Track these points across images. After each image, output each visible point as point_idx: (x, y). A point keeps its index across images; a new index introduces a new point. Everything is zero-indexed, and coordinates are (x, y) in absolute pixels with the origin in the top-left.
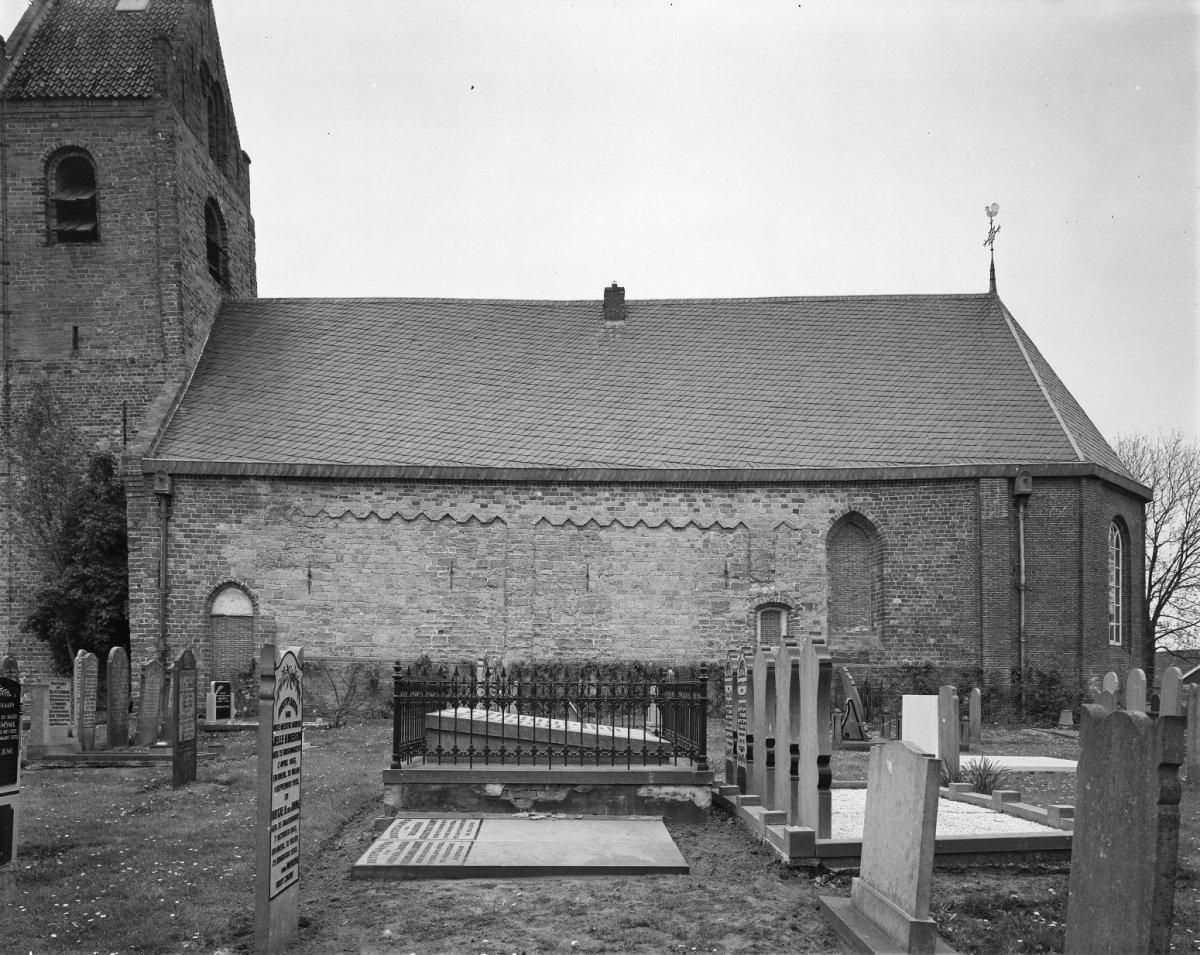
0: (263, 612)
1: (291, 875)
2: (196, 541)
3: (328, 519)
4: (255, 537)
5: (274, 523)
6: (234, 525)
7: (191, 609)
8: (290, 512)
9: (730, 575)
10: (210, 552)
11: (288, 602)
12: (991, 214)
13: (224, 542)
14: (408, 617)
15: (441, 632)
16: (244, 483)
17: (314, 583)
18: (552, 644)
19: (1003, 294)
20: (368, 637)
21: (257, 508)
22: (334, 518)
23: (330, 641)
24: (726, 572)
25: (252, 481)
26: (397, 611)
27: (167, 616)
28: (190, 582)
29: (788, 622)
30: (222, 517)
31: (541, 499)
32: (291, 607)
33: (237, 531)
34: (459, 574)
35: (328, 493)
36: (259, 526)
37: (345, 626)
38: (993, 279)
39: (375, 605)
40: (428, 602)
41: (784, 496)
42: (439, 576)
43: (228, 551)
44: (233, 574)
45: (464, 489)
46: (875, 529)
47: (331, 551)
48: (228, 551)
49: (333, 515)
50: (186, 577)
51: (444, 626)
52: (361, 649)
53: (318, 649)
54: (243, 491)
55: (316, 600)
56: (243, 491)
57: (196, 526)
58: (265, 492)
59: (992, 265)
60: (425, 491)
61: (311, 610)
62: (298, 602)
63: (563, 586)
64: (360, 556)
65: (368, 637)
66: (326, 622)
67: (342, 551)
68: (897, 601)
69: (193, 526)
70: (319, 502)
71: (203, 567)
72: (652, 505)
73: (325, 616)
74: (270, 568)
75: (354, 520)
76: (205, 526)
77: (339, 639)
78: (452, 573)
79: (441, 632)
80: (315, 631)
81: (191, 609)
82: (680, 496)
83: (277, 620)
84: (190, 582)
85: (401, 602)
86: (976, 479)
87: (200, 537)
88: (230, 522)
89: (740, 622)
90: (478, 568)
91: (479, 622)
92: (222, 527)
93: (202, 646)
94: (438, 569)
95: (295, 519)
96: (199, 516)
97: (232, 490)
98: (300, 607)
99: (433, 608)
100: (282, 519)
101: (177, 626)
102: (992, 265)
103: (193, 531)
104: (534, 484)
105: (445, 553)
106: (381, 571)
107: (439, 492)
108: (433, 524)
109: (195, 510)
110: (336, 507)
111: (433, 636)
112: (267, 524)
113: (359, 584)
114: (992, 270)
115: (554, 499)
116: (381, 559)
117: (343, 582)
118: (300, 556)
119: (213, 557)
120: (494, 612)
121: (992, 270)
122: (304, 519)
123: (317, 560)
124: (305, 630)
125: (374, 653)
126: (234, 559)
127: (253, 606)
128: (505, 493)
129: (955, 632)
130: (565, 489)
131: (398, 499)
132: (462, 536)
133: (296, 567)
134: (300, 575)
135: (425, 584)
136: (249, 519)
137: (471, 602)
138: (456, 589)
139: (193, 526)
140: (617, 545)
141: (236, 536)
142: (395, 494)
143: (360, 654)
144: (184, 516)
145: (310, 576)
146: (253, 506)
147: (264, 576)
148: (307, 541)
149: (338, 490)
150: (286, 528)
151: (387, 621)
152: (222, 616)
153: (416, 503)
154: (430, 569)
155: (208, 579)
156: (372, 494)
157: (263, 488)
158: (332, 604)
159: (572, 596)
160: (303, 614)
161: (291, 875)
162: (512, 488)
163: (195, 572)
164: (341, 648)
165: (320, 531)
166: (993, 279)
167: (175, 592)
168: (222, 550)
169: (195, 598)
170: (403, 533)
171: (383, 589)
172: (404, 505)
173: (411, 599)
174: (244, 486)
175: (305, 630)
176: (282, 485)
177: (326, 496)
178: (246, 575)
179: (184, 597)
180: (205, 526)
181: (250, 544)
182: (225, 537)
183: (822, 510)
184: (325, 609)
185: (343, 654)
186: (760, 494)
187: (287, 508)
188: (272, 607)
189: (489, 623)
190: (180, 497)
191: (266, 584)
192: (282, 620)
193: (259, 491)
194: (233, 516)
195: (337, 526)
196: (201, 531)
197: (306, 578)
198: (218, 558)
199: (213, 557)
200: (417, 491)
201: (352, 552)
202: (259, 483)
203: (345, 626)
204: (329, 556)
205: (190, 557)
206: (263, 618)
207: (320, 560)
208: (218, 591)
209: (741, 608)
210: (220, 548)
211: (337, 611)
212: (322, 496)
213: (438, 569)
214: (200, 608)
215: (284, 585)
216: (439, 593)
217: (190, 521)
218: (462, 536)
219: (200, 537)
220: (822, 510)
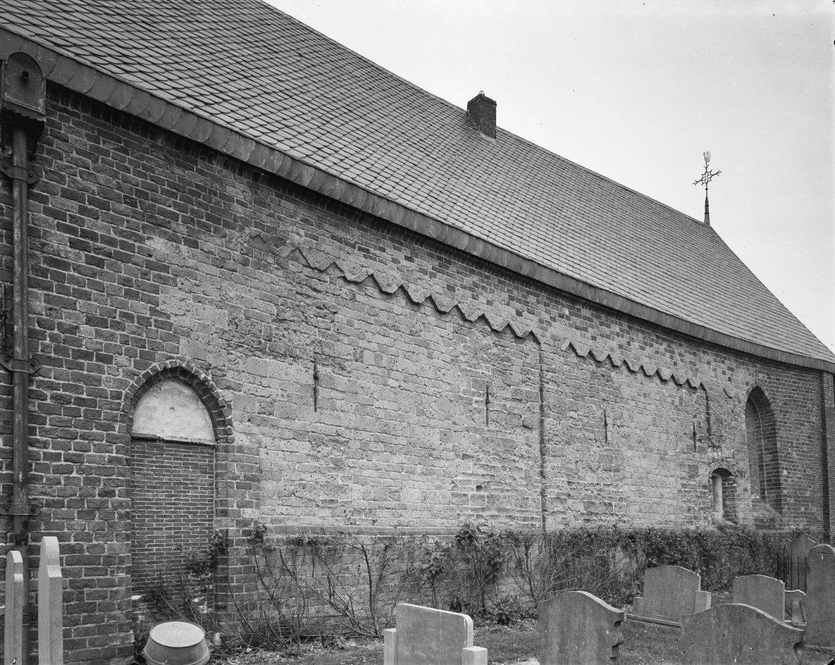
0: (239, 439)
1: (149, 546)
2: (100, 263)
3: (341, 281)
4: (225, 284)
5: (258, 266)
6: (183, 247)
7: (92, 418)
8: (285, 252)
9: (698, 437)
10: (133, 295)
11: (283, 422)
12: (707, 160)
13: (165, 281)
14: (442, 463)
15: (479, 488)
16: (201, 165)
17: (323, 393)
18: (581, 508)
19: (712, 224)
20: (394, 494)
21: (227, 225)
22: (350, 282)
23: (341, 498)
24: (695, 434)
25: (217, 167)
26: (429, 453)
27: (32, 431)
28: (87, 355)
29: (723, 488)
30: (159, 224)
31: (568, 318)
32: (287, 434)
33: (191, 262)
34: (495, 404)
35: (341, 234)
36: (231, 264)
37: (365, 473)
38: (707, 213)
39: (404, 441)
40: (466, 443)
41: (723, 362)
42: (475, 405)
43: (172, 300)
44: (184, 354)
45: (500, 282)
46: (769, 405)
47: (346, 340)
48: (172, 300)
49: (350, 277)
50: (78, 342)
51: (482, 480)
52: (386, 513)
53: (326, 513)
54: (199, 180)
55: (322, 422)
56: (199, 180)
57: (100, 227)
58: (241, 197)
59: (707, 201)
60: (461, 273)
61: (317, 442)
62: (297, 424)
63: (587, 434)
64: (385, 358)
65: (394, 494)
66: (338, 465)
67: (362, 343)
68: (785, 472)
69: (88, 223)
70: (330, 247)
71: (117, 326)
72: (648, 350)
73: (336, 454)
74: (252, 351)
75: (376, 293)
76: (121, 233)
77: (356, 495)
78: (487, 402)
79: (479, 488)
80: (323, 479)
81: (92, 418)
82: (665, 345)
83: (263, 456)
84: (87, 355)
85: (435, 439)
86: (820, 372)
87: (109, 255)
88: (173, 239)
89: (705, 487)
90: (514, 400)
91: (516, 475)
92: (158, 245)
93: (121, 505)
94: (474, 394)
95: (293, 266)
96: (104, 206)
97: (178, 171)
98: (299, 435)
99: (469, 452)
100: (270, 260)
101: (57, 457)
102: (707, 201)
103: (94, 237)
104: (564, 298)
105: (480, 371)
106: (410, 386)
107: (476, 278)
108: (467, 325)
109: (94, 188)
110: (355, 264)
111: (470, 493)
112: (245, 263)
113: (385, 404)
114: (707, 206)
115: (578, 321)
116: (412, 367)
117: (363, 397)
118: (301, 339)
119: (140, 307)
120: (530, 463)
121: (707, 206)
122: (307, 271)
123: (327, 350)
124: (307, 477)
125: (404, 520)
126: (187, 321)
127: (215, 425)
128: (538, 302)
129: (813, 502)
130: (586, 312)
131: (432, 276)
132: (495, 350)
133: (295, 358)
134: (300, 374)
135: (458, 412)
136: (211, 243)
137: (509, 447)
138: (492, 427)
139: (88, 223)
140: (626, 392)
141: (190, 273)
142: (429, 264)
143: (386, 521)
144: (67, 195)
145: (316, 378)
146: (218, 220)
147: (241, 367)
148: (311, 312)
149: (355, 234)
150: (272, 279)
151: (419, 469)
152: (152, 440)
153: (451, 288)
154: (464, 392)
155: (130, 354)
156: (400, 255)
157: (237, 189)
158: (347, 433)
159: (595, 449)
160: (304, 447)
161: (149, 546)
162: (544, 296)
163: (98, 334)
164: (359, 511)
165: (329, 300)
166: (707, 213)
167: (51, 374)
168: (161, 297)
169: (102, 394)
170: (439, 332)
171: (413, 417)
172: (501, 314)
173: (445, 436)
174: (201, 172)
175: (307, 477)
176: (271, 196)
177: (340, 240)
178: (211, 359)
179: (77, 389)
180: (121, 233)
181: (215, 296)
182: (166, 269)
183: (742, 380)
184: (336, 440)
185: (363, 523)
186: (709, 357)
187: (281, 241)
188: (255, 430)
189: (525, 478)
190: (57, 145)
191: (244, 380)
192: (271, 457)
193: (230, 191)
194: (182, 229)
195: (353, 298)
196: (111, 242)
197: (311, 382)
198: (153, 311)
199: (140, 307)
200: (452, 269)
201: (374, 346)
202: (229, 176)
203: (365, 473)
204: (342, 348)
205: (87, 296)
206: (241, 449)
207: (331, 353)
208: (151, 382)
209: (705, 473)
210: (156, 291)
211: (354, 445)
212: (333, 237)
213: (474, 394)
214: (114, 419)
215: (275, 391)
216: (476, 430)
217: (83, 210)
218: (495, 350)
219: (109, 255)
220: (742, 380)
